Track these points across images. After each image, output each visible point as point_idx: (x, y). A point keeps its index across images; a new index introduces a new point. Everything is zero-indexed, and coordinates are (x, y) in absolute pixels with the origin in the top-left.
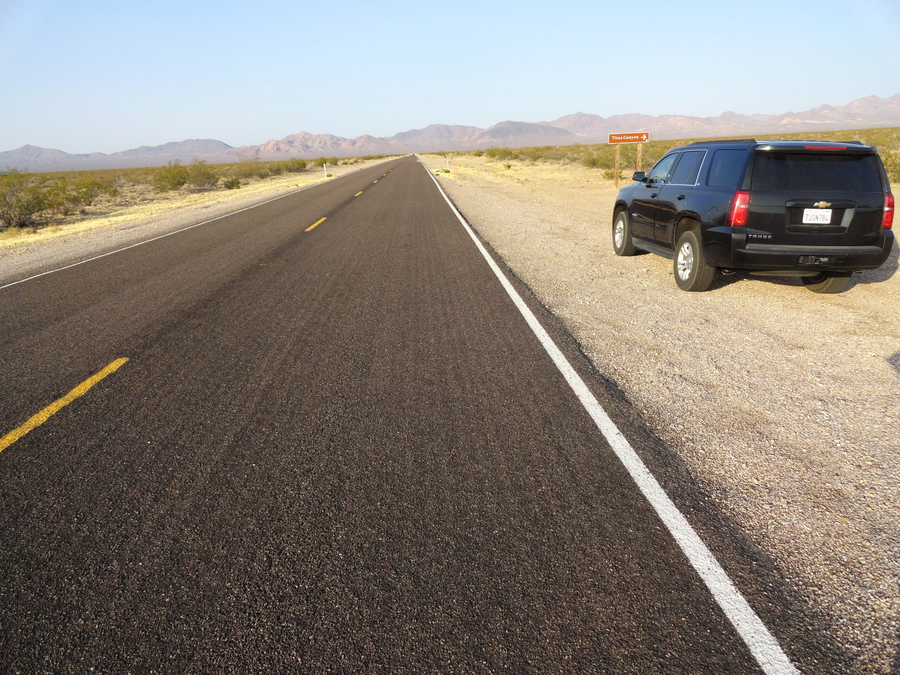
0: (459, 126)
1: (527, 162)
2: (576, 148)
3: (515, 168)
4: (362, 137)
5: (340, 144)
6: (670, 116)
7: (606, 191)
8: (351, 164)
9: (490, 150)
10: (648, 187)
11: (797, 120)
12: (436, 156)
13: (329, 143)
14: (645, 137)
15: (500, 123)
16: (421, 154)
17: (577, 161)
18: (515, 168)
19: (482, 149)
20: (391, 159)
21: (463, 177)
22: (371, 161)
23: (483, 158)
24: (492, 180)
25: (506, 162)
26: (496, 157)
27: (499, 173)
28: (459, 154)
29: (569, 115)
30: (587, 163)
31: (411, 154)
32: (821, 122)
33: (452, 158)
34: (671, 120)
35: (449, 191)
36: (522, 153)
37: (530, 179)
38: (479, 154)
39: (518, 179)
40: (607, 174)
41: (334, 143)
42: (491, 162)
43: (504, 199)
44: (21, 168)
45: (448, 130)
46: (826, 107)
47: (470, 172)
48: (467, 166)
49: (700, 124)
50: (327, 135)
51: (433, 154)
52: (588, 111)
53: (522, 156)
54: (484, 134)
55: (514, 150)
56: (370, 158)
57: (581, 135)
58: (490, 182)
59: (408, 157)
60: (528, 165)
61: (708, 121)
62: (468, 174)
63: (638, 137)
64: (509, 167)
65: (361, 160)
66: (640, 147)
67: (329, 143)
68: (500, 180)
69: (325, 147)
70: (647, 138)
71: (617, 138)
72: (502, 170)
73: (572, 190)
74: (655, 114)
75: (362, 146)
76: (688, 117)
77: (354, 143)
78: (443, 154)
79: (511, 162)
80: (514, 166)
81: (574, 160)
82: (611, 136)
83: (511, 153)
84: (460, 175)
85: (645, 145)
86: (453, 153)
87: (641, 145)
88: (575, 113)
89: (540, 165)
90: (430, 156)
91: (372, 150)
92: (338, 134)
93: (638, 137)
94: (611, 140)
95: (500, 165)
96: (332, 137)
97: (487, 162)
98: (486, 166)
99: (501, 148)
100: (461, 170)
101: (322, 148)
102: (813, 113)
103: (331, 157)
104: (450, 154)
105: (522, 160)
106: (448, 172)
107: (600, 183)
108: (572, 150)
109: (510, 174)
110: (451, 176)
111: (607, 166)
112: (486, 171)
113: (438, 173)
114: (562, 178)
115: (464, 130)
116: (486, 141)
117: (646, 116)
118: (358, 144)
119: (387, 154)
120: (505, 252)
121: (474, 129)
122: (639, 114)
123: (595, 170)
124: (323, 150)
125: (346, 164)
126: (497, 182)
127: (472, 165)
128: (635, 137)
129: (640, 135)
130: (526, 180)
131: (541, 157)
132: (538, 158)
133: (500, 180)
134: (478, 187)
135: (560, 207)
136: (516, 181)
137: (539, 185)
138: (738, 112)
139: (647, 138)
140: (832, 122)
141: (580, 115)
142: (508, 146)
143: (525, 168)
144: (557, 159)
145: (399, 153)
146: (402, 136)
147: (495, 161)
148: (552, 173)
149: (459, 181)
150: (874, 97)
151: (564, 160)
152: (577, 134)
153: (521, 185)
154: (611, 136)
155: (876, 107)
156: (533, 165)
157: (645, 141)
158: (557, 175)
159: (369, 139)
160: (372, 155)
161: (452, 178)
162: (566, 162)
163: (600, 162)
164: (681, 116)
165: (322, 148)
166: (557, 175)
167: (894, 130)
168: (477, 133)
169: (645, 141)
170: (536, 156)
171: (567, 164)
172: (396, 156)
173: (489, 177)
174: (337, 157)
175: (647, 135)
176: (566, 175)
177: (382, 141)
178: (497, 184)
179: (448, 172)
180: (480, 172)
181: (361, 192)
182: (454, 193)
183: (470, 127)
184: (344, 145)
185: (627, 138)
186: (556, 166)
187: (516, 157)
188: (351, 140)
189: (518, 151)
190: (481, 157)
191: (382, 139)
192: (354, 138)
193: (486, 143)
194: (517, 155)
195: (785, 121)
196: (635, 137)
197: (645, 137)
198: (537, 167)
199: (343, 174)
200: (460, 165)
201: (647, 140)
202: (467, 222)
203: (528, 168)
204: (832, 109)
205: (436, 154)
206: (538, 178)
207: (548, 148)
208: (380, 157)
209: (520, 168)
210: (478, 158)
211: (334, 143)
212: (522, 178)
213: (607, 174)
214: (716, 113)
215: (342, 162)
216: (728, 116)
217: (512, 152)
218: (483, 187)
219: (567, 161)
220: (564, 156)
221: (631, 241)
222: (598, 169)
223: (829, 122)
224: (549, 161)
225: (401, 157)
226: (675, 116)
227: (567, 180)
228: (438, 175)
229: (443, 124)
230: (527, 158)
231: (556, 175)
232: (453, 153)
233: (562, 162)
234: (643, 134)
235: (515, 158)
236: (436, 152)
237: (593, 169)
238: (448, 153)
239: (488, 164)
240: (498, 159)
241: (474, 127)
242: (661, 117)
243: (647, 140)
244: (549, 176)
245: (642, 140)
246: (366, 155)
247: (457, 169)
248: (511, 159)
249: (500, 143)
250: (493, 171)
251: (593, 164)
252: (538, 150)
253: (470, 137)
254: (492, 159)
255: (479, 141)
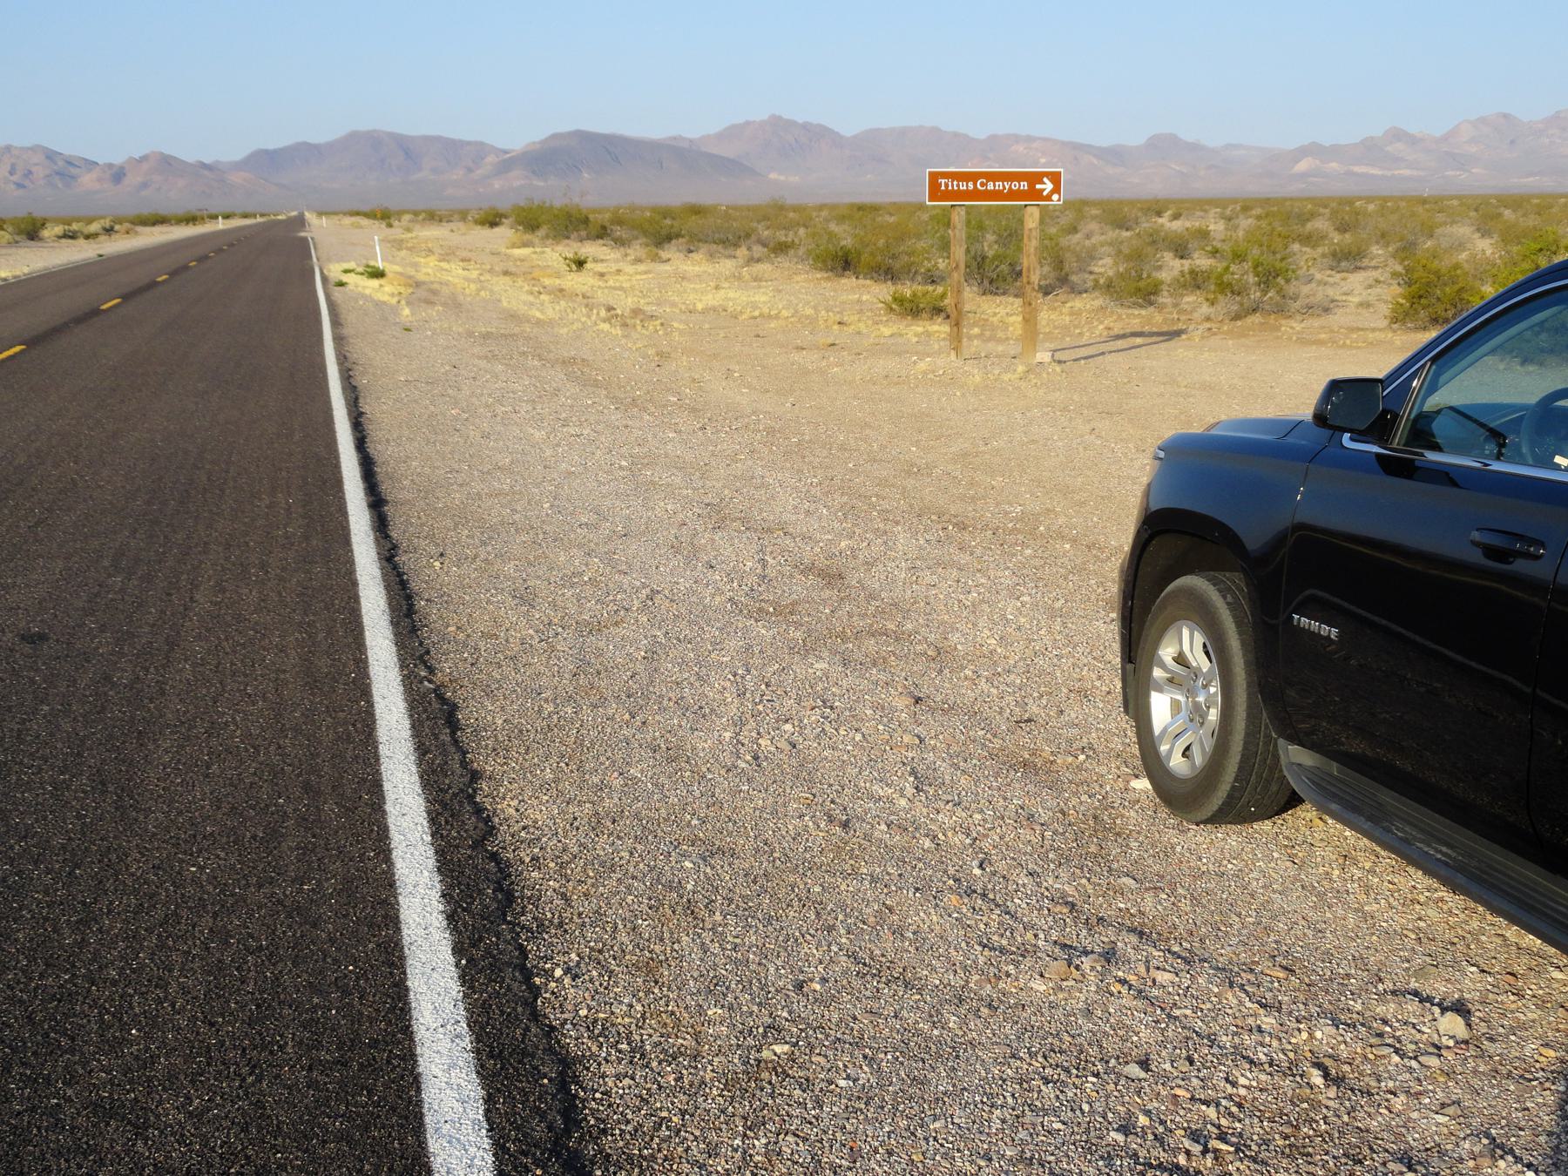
0: (438, 139)
1: (637, 250)
2: (775, 213)
3: (600, 267)
4: (144, 158)
5: (73, 177)
6: (1016, 139)
7: (922, 366)
8: (87, 237)
9: (523, 209)
10: (1389, 465)
11: (1334, 165)
12: (364, 222)
13: (40, 172)
14: (1048, 186)
15: (555, 136)
16: (320, 214)
17: (792, 252)
18: (600, 267)
19: (503, 205)
20: (221, 225)
21: (423, 293)
22: (157, 229)
23: (504, 233)
24: (523, 309)
25: (570, 249)
26: (541, 232)
27: (547, 282)
28: (433, 217)
29: (748, 123)
30: (824, 261)
31: (294, 213)
32: (1389, 173)
33: (408, 230)
34: (1021, 148)
35: (360, 350)
36: (619, 222)
37: (649, 309)
38: (492, 221)
39: (610, 309)
40: (899, 300)
41: (58, 173)
42: (525, 245)
43: (556, 392)
44: (1269, 196)
45: (407, 150)
46: (1397, 135)
47: (455, 275)
48: (448, 255)
49: (1095, 161)
50: (35, 149)
51: (358, 214)
52: (800, 112)
53: (619, 232)
54: (509, 163)
55: (594, 211)
56: (159, 220)
57: (782, 178)
58: (513, 317)
59: (280, 222)
60: (638, 261)
61: (1115, 154)
62: (447, 284)
63: (1024, 185)
64: (580, 264)
65: (127, 225)
66: (1032, 218)
67: (40, 172)
68: (550, 310)
69: (27, 183)
70: (1056, 190)
71: (954, 185)
72: (558, 275)
73: (796, 357)
74: (979, 132)
75: (145, 185)
76: (1064, 144)
77: (118, 174)
78: (385, 216)
79: (589, 249)
80: (595, 261)
81: (781, 248)
82: (934, 177)
83: (586, 221)
84: (418, 284)
85: (1046, 216)
86: (416, 213)
87: (1036, 212)
88: (765, 117)
89: (677, 261)
90: (348, 220)
91: (175, 198)
92: (68, 146)
93: (1024, 185)
94: (935, 193)
95: (554, 255)
96: (51, 156)
97: (514, 246)
98: (508, 257)
99: (558, 204)
100: (429, 268)
101: (20, 186)
102: (1370, 149)
103: (21, 213)
104: (407, 217)
105: (620, 242)
106: (378, 274)
107: (886, 331)
108: (766, 218)
109: (581, 289)
110: (388, 289)
111: (887, 272)
112: (506, 273)
113: (345, 278)
114: (755, 306)
115: (451, 148)
116: (516, 183)
117: (956, 135)
118: (132, 180)
119: (214, 211)
120: (541, 812)
121: (480, 150)
122: (935, 131)
123: (849, 282)
124: (21, 192)
125: (71, 236)
126: (538, 314)
127: (465, 254)
128: (1015, 186)
129: (1036, 178)
130: (636, 312)
131: (678, 236)
132: (669, 238)
133: (550, 310)
134: (470, 334)
135: (771, 431)
136: (603, 313)
137: (681, 332)
138: (1188, 136)
139: (1056, 190)
140: (1415, 173)
141: (777, 123)
142: (576, 200)
143: (630, 269)
144: (724, 242)
145: (250, 209)
146: (266, 161)
147: (536, 241)
148: (717, 288)
149: (407, 311)
150: (1506, 116)
151: (749, 249)
152: (773, 176)
153: (618, 331)
154: (934, 177)
155: (1512, 142)
156: (655, 258)
157: (1049, 198)
158: (734, 297)
159: (167, 164)
160: (163, 211)
161: (385, 298)
162: (756, 256)
163: (865, 257)
164: (1045, 140)
165: (20, 186)
166: (734, 297)
167: (1562, 196)
168: (491, 159)
169: (1049, 198)
170: (664, 232)
171: (759, 260)
172: (245, 216)
173: (514, 295)
174: (39, 213)
175: (1055, 178)
176: (762, 297)
177: (206, 172)
178: (539, 323)
179: (378, 274)
180: (487, 276)
181: (18, 349)
182: (373, 357)
183: (469, 143)
184: (88, 180)
185: (990, 186)
186: (727, 266)
187: (602, 233)
188: (110, 166)
189: (607, 216)
190: (496, 230)
191: (204, 166)
192: (118, 159)
193: (514, 188)
194: (604, 228)
195: (1302, 166)
196: (1015, 186)
197: (1048, 186)
198: (667, 267)
199: (26, 270)
200: (430, 251)
201: (1055, 197)
202: (381, 524)
203: (641, 267)
204: (1412, 140)
205: (367, 215)
206: (674, 305)
207: (697, 210)
208: (191, 219)
209: (614, 267)
210: (486, 232)
211: (58, 173)
212: (625, 304)
213: (899, 300)
214: (1134, 136)
215: (59, 230)
216: (1163, 146)
217: (591, 217)
218: (486, 336)
219: (758, 250)
220: (748, 236)
221: (1276, 757)
222: (861, 282)
223: (1407, 172)
224: (704, 248)
225: (259, 220)
226: (1030, 139)
227: (770, 317)
228: (341, 284)
229: (389, 130)
230: (637, 238)
231: (731, 294)
232: (416, 213)
233: (742, 252)
234: (1046, 174)
235: (599, 237)
236: (366, 208)
237: (844, 281)
238: (400, 214)
239: (518, 252)
240: (547, 237)
241: (482, 144)
242: (993, 138)
243: (1055, 197)
244: (711, 299)
245: (1038, 195)
246: (146, 211)
247: (416, 265)
248: (588, 238)
249: (554, 191)
250: (531, 275)
251: (844, 263)
252: (666, 213)
253: (470, 170)
254: (528, 237)
255: (497, 185)
